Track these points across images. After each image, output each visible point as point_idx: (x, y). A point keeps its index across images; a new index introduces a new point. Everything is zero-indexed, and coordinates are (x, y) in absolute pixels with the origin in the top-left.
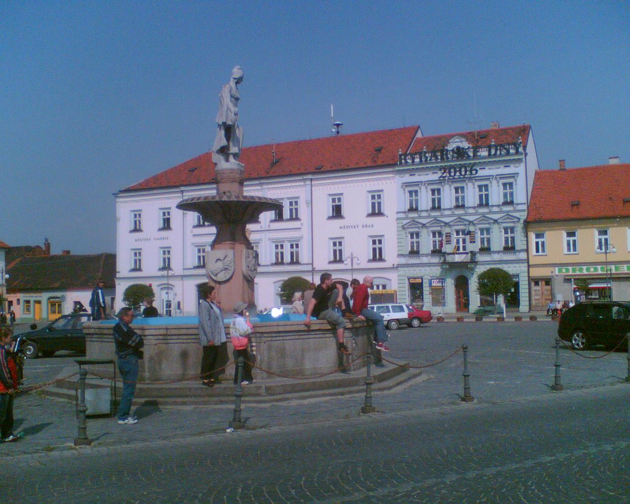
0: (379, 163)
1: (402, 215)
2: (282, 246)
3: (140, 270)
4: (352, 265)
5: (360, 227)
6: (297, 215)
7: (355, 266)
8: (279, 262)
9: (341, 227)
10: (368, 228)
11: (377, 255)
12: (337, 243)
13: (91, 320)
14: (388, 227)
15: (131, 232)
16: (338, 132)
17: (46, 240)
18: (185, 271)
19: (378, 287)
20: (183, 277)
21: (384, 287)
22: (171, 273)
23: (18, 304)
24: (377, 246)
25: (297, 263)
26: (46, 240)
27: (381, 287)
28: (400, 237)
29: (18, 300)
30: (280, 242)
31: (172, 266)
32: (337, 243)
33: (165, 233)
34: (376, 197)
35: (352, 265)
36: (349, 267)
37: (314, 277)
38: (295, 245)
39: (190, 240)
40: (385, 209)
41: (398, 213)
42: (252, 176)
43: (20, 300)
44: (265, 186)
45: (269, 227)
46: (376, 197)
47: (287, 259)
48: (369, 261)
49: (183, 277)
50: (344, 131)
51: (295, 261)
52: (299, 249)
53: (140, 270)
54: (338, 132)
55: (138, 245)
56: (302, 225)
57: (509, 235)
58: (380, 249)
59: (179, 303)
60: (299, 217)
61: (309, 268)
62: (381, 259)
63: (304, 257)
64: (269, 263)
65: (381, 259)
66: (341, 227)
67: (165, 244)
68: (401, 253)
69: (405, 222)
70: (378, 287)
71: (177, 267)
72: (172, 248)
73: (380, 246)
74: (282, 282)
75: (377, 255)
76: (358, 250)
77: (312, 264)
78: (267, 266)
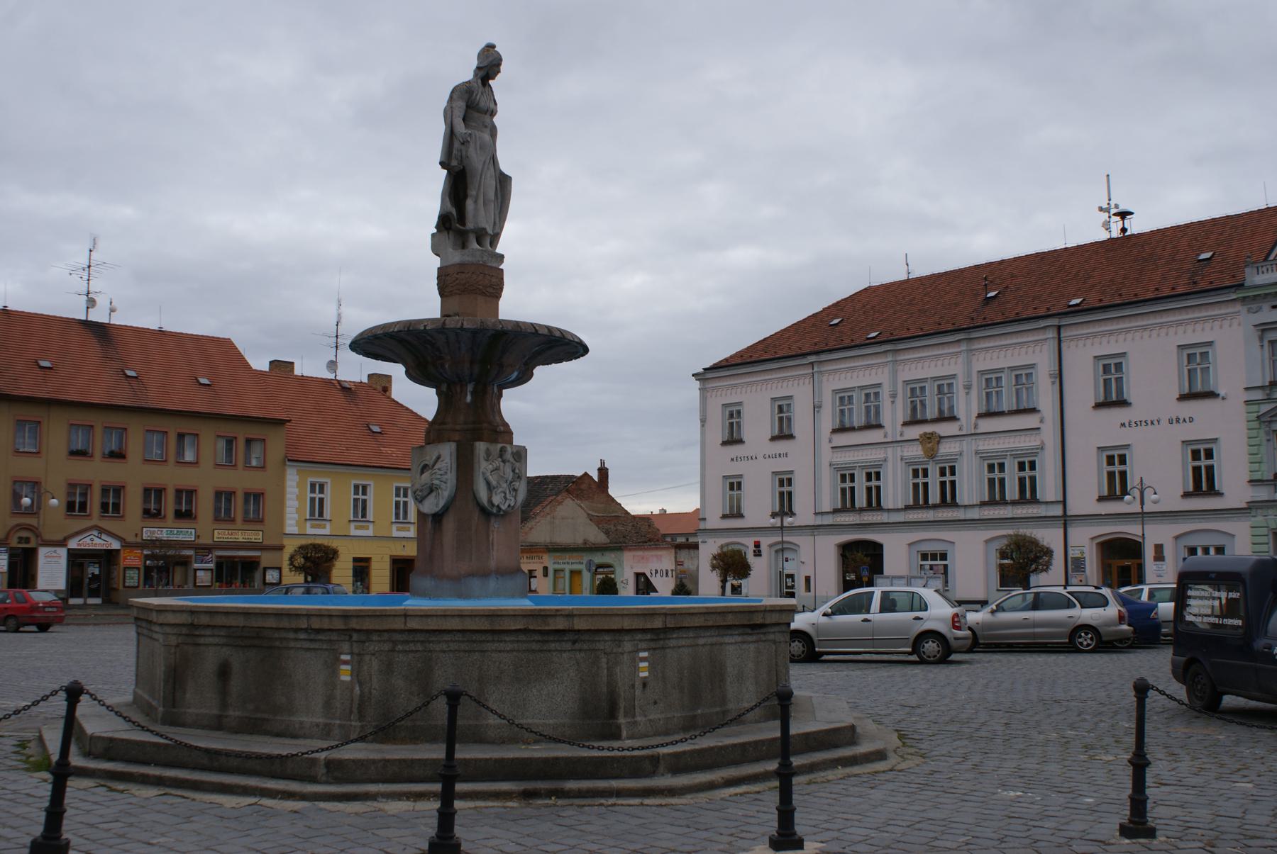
0: (1204, 285)
1: (1258, 395)
2: (1002, 466)
3: (740, 515)
4: (1142, 503)
5: (1164, 422)
6: (1120, 390)
7: (1149, 507)
8: (996, 497)
9: (1123, 425)
10: (1182, 425)
11: (1203, 482)
12: (1116, 459)
13: (586, 593)
14: (1228, 425)
15: (724, 443)
16: (1124, 230)
17: (602, 463)
18: (819, 517)
19: (1206, 550)
20: (814, 529)
21: (1220, 550)
22: (788, 521)
23: (546, 575)
24: (1203, 463)
25: (1034, 500)
26: (602, 463)
27: (1212, 551)
28: (1253, 442)
29: (546, 569)
30: (1026, 455)
31: (796, 508)
32: (1116, 459)
33: (782, 446)
34: (1196, 357)
35: (1142, 503)
36: (1136, 508)
37: (1070, 530)
38: (1027, 464)
39: (827, 456)
40: (796, 430)
41: (1247, 389)
42: (943, 328)
43: (139, 512)
44: (901, 357)
45: (976, 426)
46: (1196, 357)
47: (1012, 492)
48: (1186, 495)
49: (814, 529)
50: (1136, 226)
51: (1028, 494)
52: (1037, 473)
53: (740, 515)
54: (1124, 230)
55: (734, 469)
56: (1041, 421)
57: (361, 497)
58: (1033, 479)
59: (808, 579)
60: (1125, 396)
61: (1058, 511)
62: (1212, 491)
63: (1048, 488)
64: (976, 501)
65: (1212, 491)
66: (1123, 425)
67: (781, 465)
68: (1257, 476)
69: (1265, 408)
70: (1206, 550)
71: (804, 513)
72: (745, 477)
73: (1122, 468)
74: (1005, 541)
75: (1203, 482)
76: (1161, 475)
77: (1064, 502)
78: (973, 506)
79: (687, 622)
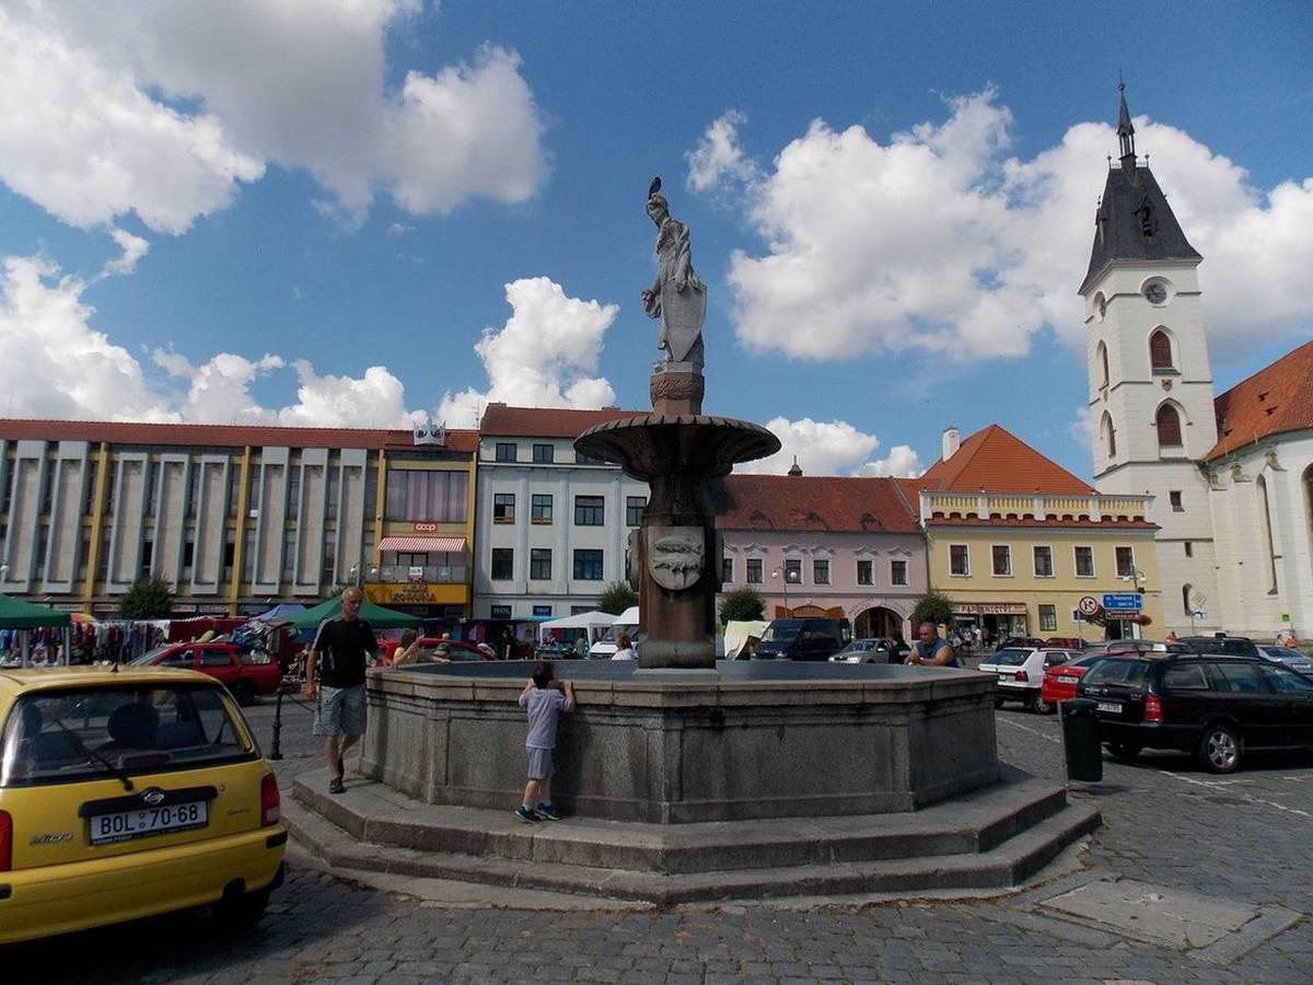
79: (812, 711)
